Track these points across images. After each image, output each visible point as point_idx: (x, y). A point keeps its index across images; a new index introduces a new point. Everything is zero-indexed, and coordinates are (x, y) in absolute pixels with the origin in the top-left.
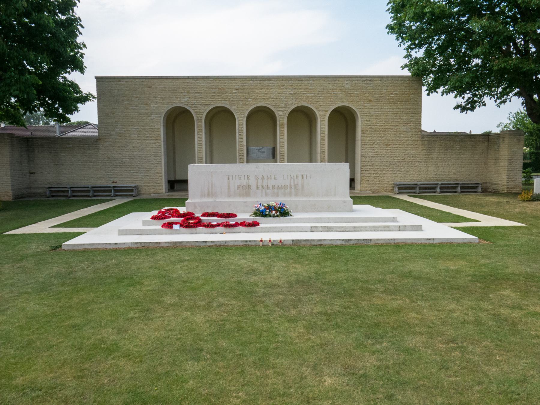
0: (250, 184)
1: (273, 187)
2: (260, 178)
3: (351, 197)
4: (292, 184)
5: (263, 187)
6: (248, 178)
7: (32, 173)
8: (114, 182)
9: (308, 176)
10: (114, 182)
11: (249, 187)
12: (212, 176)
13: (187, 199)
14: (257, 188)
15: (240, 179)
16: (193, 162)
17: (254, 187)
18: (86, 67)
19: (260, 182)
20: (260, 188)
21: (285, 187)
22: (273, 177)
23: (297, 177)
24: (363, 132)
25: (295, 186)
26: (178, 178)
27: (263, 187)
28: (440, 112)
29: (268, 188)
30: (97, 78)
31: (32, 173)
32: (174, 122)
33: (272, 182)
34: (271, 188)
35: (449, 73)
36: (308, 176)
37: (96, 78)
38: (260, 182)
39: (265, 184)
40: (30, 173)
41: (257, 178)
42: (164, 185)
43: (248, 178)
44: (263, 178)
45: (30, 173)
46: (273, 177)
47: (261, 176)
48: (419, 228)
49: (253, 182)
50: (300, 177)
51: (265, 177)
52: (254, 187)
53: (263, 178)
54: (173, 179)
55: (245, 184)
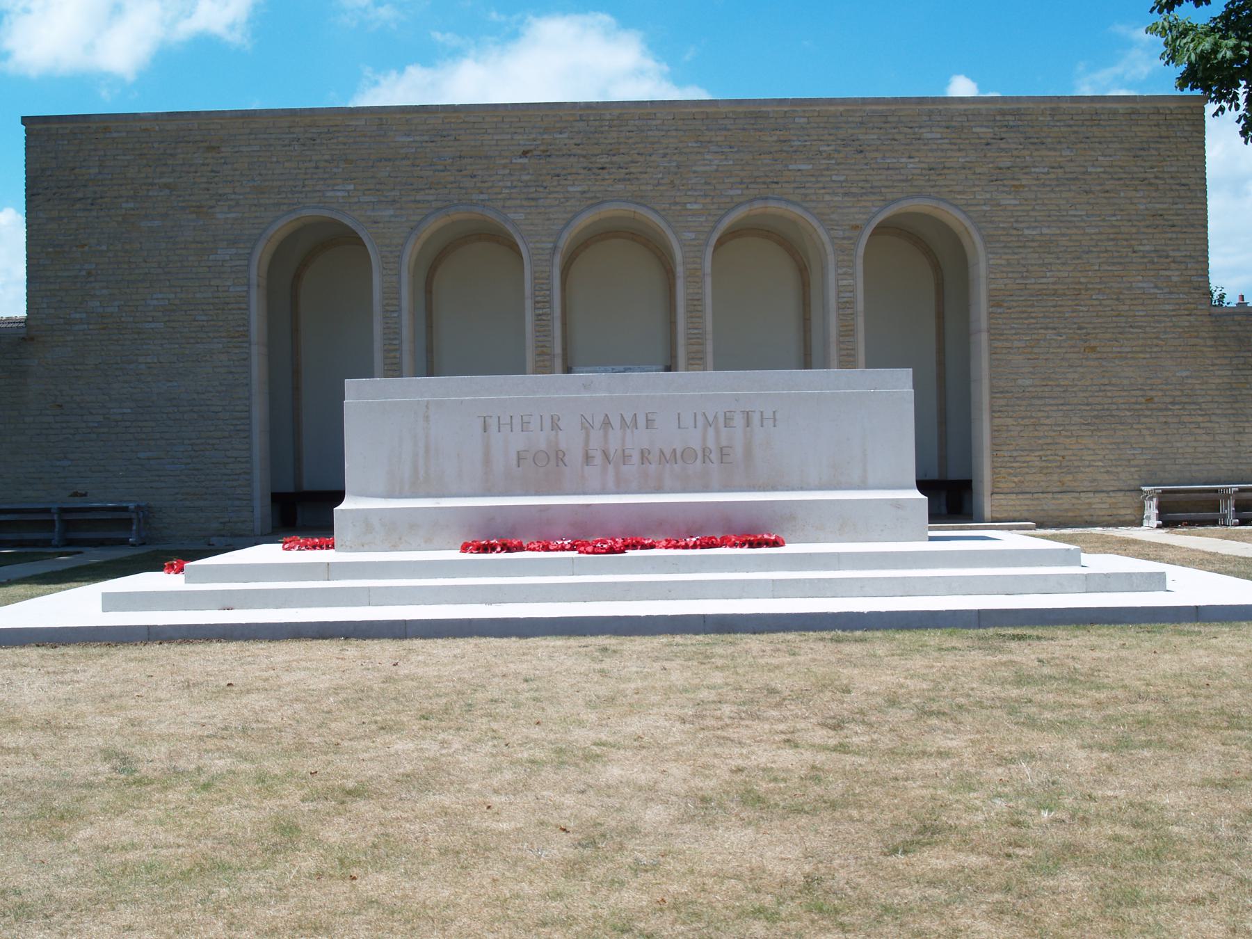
0: (563, 446)
1: (644, 456)
2: (597, 425)
3: (922, 486)
4: (711, 443)
5: (605, 454)
6: (555, 426)
8: (75, 495)
10: (75, 495)
11: (559, 457)
12: (427, 418)
13: (339, 497)
14: (588, 459)
15: (524, 426)
19: (596, 435)
20: (598, 459)
21: (686, 455)
22: (642, 421)
23: (728, 420)
25: (723, 452)
26: (307, 486)
27: (605, 454)
29: (625, 458)
30: (26, 120)
34: (636, 458)
37: (26, 120)
38: (596, 435)
39: (614, 446)
41: (586, 426)
42: (257, 504)
44: (607, 423)
46: (642, 421)
48: (1157, 581)
49: (571, 441)
50: (739, 421)
51: (616, 422)
53: (607, 423)
54: (289, 488)
55: (543, 446)
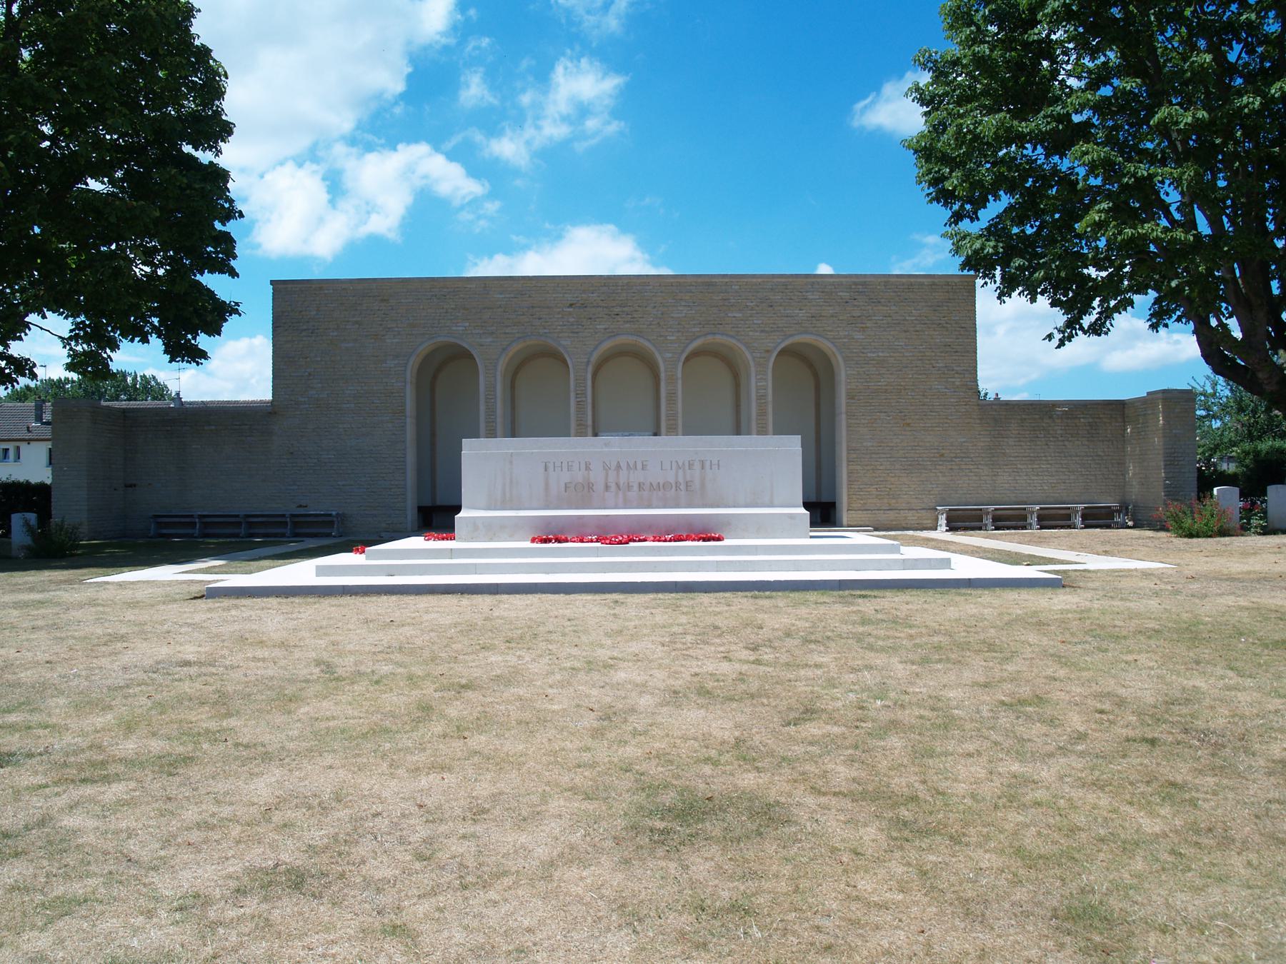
0: (592, 480)
4: (681, 479)
5: (618, 485)
6: (588, 468)
7: (131, 486)
9: (715, 462)
11: (590, 486)
12: (511, 463)
13: (458, 509)
14: (607, 488)
16: (475, 434)
17: (600, 487)
18: (237, 304)
19: (612, 474)
21: (666, 486)
22: (639, 466)
23: (691, 465)
24: (851, 396)
25: (687, 485)
26: (438, 503)
27: (618, 485)
28: (1019, 345)
29: (629, 487)
31: (131, 486)
32: (435, 377)
33: (637, 477)
34: (636, 488)
35: (1022, 236)
36: (715, 462)
37: (272, 282)
38: (612, 474)
39: (622, 481)
40: (126, 486)
41: (606, 468)
43: (588, 468)
44: (619, 467)
45: (126, 486)
46: (639, 466)
47: (614, 464)
48: (946, 564)
49: (597, 476)
50: (697, 466)
51: (624, 465)
52: (600, 487)
53: (619, 467)
